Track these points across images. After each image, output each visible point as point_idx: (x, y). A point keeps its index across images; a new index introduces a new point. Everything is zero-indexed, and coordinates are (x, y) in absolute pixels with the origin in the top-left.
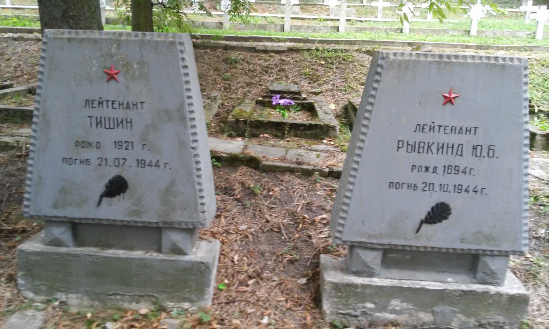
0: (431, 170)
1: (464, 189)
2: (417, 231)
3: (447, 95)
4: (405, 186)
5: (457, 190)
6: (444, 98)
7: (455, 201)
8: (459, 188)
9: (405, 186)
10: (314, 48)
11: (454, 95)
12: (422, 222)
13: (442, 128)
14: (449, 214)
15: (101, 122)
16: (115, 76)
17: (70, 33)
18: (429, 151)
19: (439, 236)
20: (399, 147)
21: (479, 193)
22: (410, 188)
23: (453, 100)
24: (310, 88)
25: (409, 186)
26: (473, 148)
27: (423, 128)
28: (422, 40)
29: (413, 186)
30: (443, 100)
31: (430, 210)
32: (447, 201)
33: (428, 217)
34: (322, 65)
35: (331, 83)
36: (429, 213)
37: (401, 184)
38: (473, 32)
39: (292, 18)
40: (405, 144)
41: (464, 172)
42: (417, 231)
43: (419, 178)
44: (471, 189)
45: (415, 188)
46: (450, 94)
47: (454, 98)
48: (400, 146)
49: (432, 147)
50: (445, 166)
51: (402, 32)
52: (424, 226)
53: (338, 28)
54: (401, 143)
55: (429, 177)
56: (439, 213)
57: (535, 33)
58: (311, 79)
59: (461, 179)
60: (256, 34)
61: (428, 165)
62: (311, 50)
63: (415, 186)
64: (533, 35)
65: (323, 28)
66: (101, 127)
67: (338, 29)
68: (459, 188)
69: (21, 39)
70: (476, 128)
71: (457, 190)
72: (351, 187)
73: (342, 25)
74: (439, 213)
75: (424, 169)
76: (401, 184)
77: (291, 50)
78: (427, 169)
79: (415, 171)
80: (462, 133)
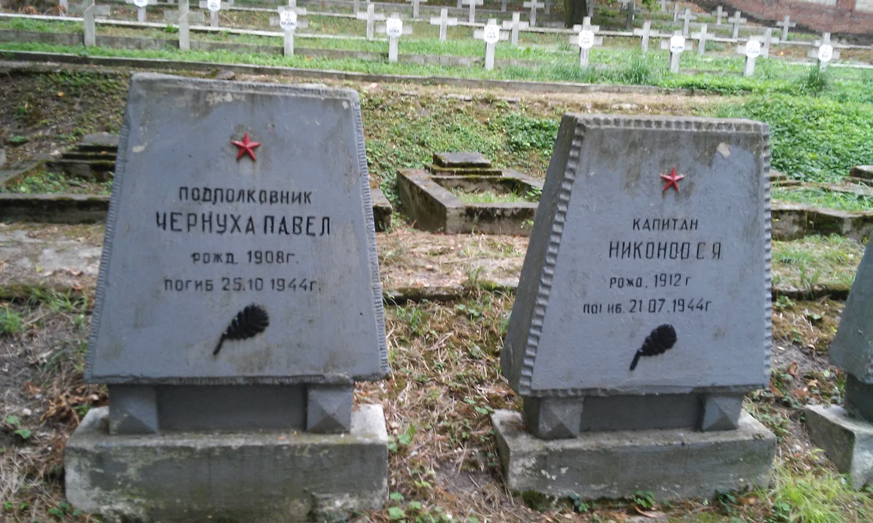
1: (286, 284)
2: (216, 352)
3: (669, 177)
4: (192, 285)
7: (679, 322)
8: (280, 284)
9: (192, 285)
10: (59, 71)
11: (677, 178)
12: (224, 338)
16: (251, 151)
17: (416, 89)
18: (236, 229)
19: (659, 373)
20: (189, 225)
21: (308, 289)
22: (199, 288)
23: (678, 185)
24: (12, 135)
28: (345, 69)
30: (235, 152)
32: (258, 302)
33: (233, 329)
34: (58, 98)
35: (54, 127)
36: (234, 322)
37: (184, 282)
38: (393, 56)
39: (191, 30)
40: (200, 219)
42: (216, 352)
44: (298, 283)
45: (209, 287)
46: (244, 140)
47: (254, 148)
48: (192, 222)
51: (283, 53)
52: (227, 344)
53: (178, 42)
54: (192, 218)
57: (484, 59)
58: (25, 121)
60: (137, 56)
61: (218, 252)
62: (51, 73)
64: (482, 63)
65: (153, 42)
66: (202, 289)
67: (176, 44)
68: (280, 284)
71: (276, 286)
73: (184, 39)
75: (212, 258)
76: (184, 282)
77: (17, 73)
80: (649, 228)
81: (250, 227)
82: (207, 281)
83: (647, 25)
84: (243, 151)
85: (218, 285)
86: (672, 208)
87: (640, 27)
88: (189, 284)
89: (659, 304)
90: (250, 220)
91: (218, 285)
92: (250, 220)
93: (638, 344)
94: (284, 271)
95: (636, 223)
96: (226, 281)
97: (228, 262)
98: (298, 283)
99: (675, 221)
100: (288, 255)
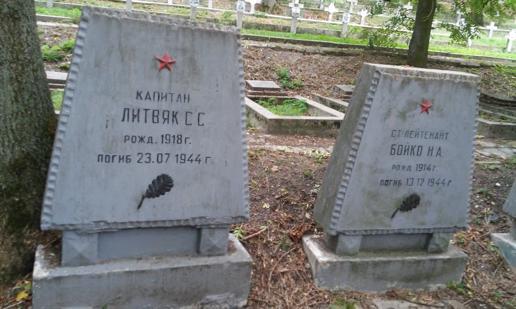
0: (146, 140)
5: (418, 169)
6: (421, 107)
8: (182, 158)
9: (116, 159)
12: (143, 198)
13: (424, 133)
14: (172, 186)
15: (405, 151)
16: (168, 65)
19: (171, 207)
21: (446, 185)
22: (121, 161)
25: (395, 183)
26: (429, 150)
27: (411, 133)
29: (125, 158)
31: (151, 183)
36: (150, 187)
41: (429, 169)
42: (139, 207)
43: (132, 149)
44: (194, 158)
47: (170, 63)
49: (177, 116)
50: (163, 136)
52: (146, 200)
55: (146, 148)
56: (162, 186)
59: (429, 175)
60: (332, 40)
63: (127, 159)
66: (123, 161)
68: (182, 158)
69: (278, 49)
70: (447, 133)
72: (345, 184)
74: (162, 186)
75: (138, 139)
78: (142, 139)
79: (129, 142)
80: (150, 98)
81: (439, 153)
82: (127, 156)
83: (493, 24)
84: (164, 64)
85: (135, 158)
86: (164, 82)
87: (488, 24)
88: (115, 158)
89: (165, 157)
90: (440, 149)
91: (135, 158)
92: (440, 149)
93: (145, 186)
94: (187, 149)
95: (139, 94)
96: (140, 155)
97: (148, 142)
98: (194, 158)
99: (172, 94)
100: (186, 138)
